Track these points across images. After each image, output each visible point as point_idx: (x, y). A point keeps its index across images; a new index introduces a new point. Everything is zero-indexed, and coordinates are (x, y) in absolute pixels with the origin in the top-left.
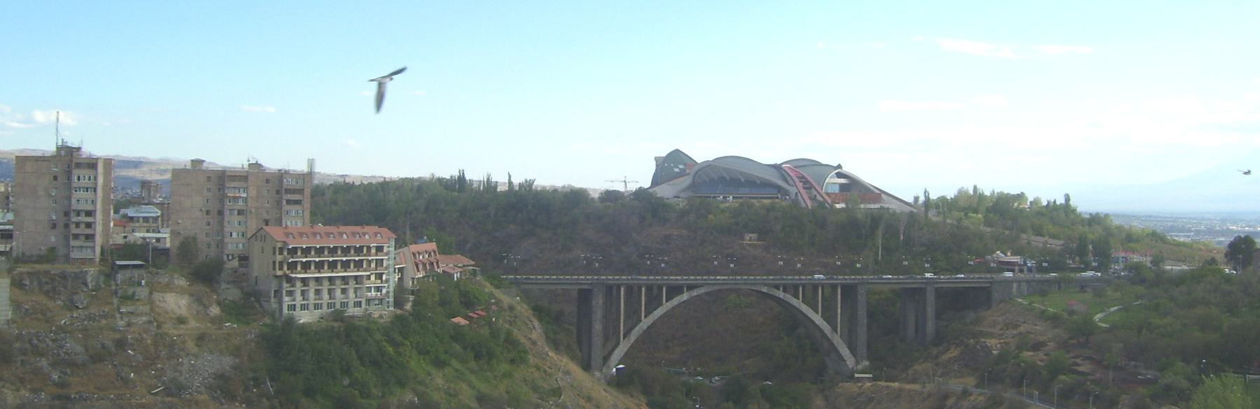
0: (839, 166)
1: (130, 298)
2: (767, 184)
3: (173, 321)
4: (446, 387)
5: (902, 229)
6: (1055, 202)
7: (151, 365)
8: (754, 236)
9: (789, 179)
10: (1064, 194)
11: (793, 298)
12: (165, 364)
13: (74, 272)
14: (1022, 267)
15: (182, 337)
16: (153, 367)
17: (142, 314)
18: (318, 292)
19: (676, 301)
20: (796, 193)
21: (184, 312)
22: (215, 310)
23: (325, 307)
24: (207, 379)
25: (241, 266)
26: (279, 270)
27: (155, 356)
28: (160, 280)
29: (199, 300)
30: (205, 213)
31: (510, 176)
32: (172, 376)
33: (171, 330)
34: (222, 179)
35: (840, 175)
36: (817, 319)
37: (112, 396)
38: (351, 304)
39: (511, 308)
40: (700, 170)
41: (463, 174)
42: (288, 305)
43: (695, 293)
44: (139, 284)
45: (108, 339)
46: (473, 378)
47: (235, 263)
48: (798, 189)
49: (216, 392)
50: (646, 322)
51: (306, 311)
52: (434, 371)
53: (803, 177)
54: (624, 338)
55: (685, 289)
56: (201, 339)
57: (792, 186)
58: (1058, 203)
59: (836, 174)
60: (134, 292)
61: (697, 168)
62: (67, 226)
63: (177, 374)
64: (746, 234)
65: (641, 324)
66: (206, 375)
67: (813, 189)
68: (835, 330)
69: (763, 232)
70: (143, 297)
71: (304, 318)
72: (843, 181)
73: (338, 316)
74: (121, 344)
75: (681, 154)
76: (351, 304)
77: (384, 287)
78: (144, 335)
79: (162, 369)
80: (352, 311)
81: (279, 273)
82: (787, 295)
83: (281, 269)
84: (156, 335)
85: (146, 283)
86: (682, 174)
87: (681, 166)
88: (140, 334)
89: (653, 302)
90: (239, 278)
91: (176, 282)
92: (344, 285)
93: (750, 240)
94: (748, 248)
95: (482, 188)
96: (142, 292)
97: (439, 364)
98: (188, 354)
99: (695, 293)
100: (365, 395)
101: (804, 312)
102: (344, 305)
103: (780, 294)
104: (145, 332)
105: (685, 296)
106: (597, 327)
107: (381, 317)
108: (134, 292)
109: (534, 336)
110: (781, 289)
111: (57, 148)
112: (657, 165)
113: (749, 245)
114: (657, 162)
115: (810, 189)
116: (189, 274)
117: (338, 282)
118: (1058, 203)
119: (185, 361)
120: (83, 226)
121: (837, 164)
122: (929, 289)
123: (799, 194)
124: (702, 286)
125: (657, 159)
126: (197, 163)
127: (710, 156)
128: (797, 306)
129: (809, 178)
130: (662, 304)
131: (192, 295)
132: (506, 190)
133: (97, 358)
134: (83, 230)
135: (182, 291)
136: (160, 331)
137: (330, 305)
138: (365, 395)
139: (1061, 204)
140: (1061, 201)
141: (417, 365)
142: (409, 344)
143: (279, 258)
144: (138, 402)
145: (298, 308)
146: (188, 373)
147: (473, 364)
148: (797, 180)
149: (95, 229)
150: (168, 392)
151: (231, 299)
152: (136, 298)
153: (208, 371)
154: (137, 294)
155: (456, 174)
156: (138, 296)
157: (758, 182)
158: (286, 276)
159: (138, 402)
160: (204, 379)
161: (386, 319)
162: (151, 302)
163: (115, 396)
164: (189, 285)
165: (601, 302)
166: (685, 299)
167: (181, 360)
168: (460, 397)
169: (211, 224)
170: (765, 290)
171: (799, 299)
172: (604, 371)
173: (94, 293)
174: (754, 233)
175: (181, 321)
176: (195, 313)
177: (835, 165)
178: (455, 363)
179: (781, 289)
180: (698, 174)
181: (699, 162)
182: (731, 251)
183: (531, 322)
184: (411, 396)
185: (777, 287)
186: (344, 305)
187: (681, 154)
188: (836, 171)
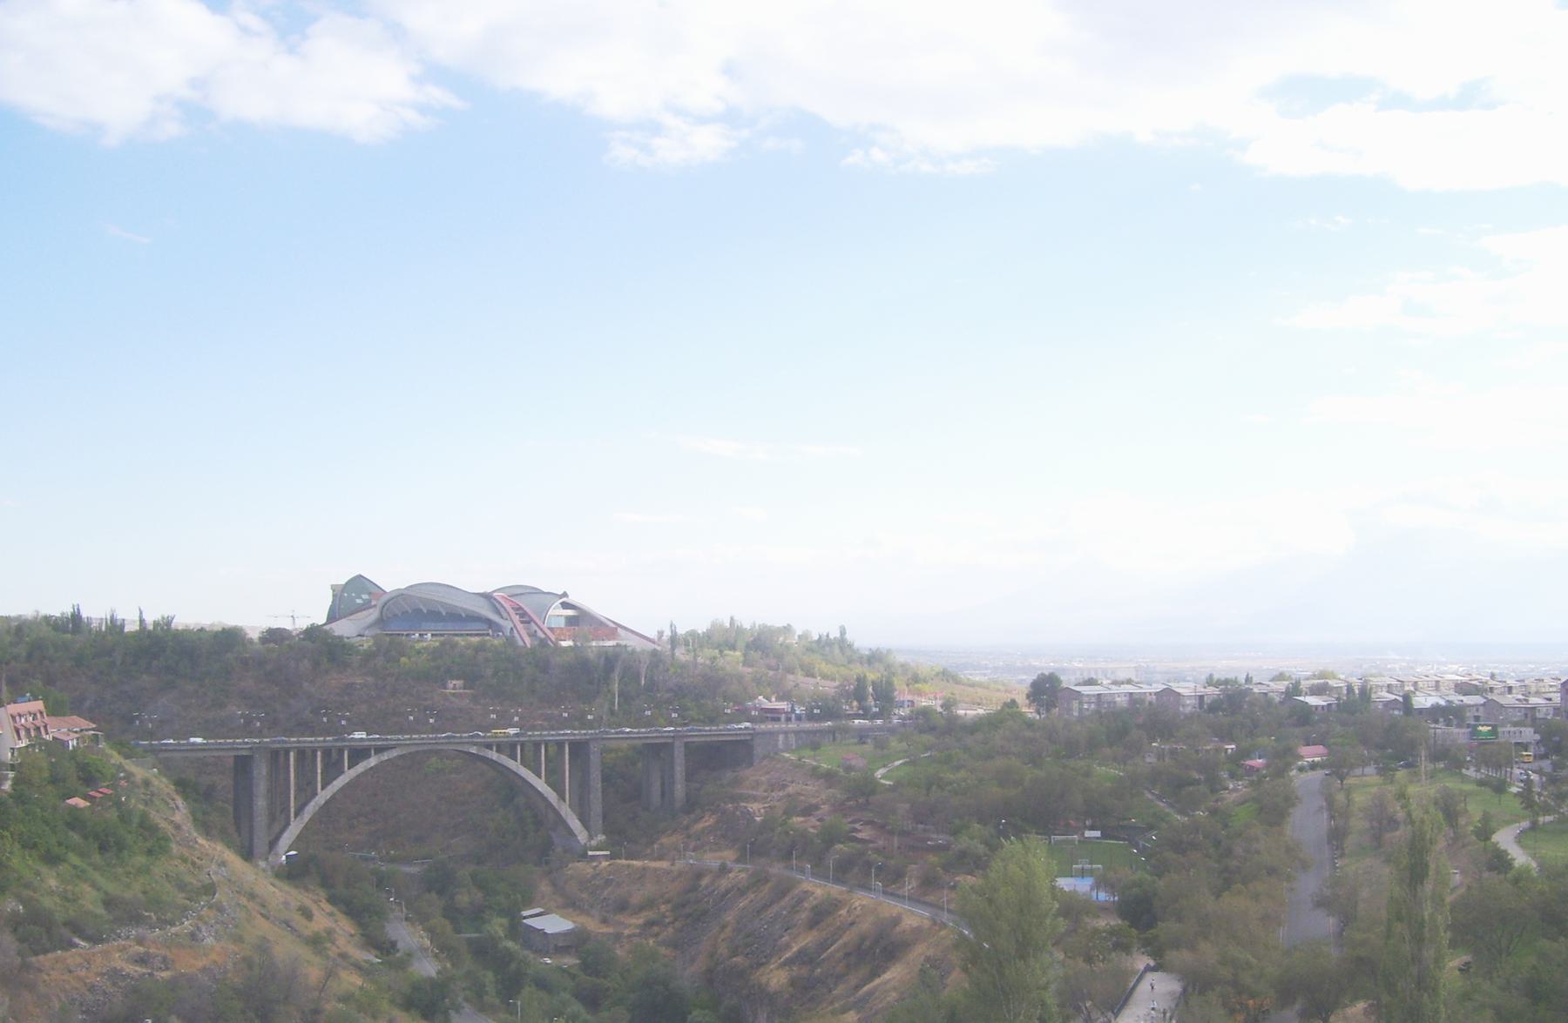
0: (565, 595)
5: (643, 671)
6: (828, 636)
8: (459, 683)
9: (502, 610)
19: (361, 767)
20: (512, 629)
31: (141, 613)
35: (565, 606)
36: (540, 785)
39: (147, 783)
41: (78, 609)
43: (385, 756)
46: (97, 876)
48: (513, 622)
50: (323, 796)
52: (44, 869)
54: (295, 817)
55: (373, 752)
61: (384, 599)
65: (317, 798)
67: (532, 624)
68: (562, 797)
69: (471, 679)
72: (570, 612)
75: (367, 582)
82: (502, 756)
86: (366, 606)
93: (454, 688)
94: (453, 699)
97: (52, 859)
99: (385, 756)
103: (493, 755)
105: (373, 761)
106: (259, 803)
109: (178, 818)
110: (494, 748)
112: (334, 596)
114: (334, 591)
115: (529, 623)
122: (677, 743)
123: (514, 630)
125: (334, 588)
130: (343, 772)
140: (835, 634)
147: (97, 858)
155: (68, 611)
157: (464, 615)
165: (264, 771)
166: (372, 765)
168: (80, 902)
170: (474, 750)
171: (516, 761)
177: (560, 593)
178: (74, 859)
181: (388, 591)
184: (14, 904)
185: (489, 746)
187: (365, 581)
188: (561, 601)
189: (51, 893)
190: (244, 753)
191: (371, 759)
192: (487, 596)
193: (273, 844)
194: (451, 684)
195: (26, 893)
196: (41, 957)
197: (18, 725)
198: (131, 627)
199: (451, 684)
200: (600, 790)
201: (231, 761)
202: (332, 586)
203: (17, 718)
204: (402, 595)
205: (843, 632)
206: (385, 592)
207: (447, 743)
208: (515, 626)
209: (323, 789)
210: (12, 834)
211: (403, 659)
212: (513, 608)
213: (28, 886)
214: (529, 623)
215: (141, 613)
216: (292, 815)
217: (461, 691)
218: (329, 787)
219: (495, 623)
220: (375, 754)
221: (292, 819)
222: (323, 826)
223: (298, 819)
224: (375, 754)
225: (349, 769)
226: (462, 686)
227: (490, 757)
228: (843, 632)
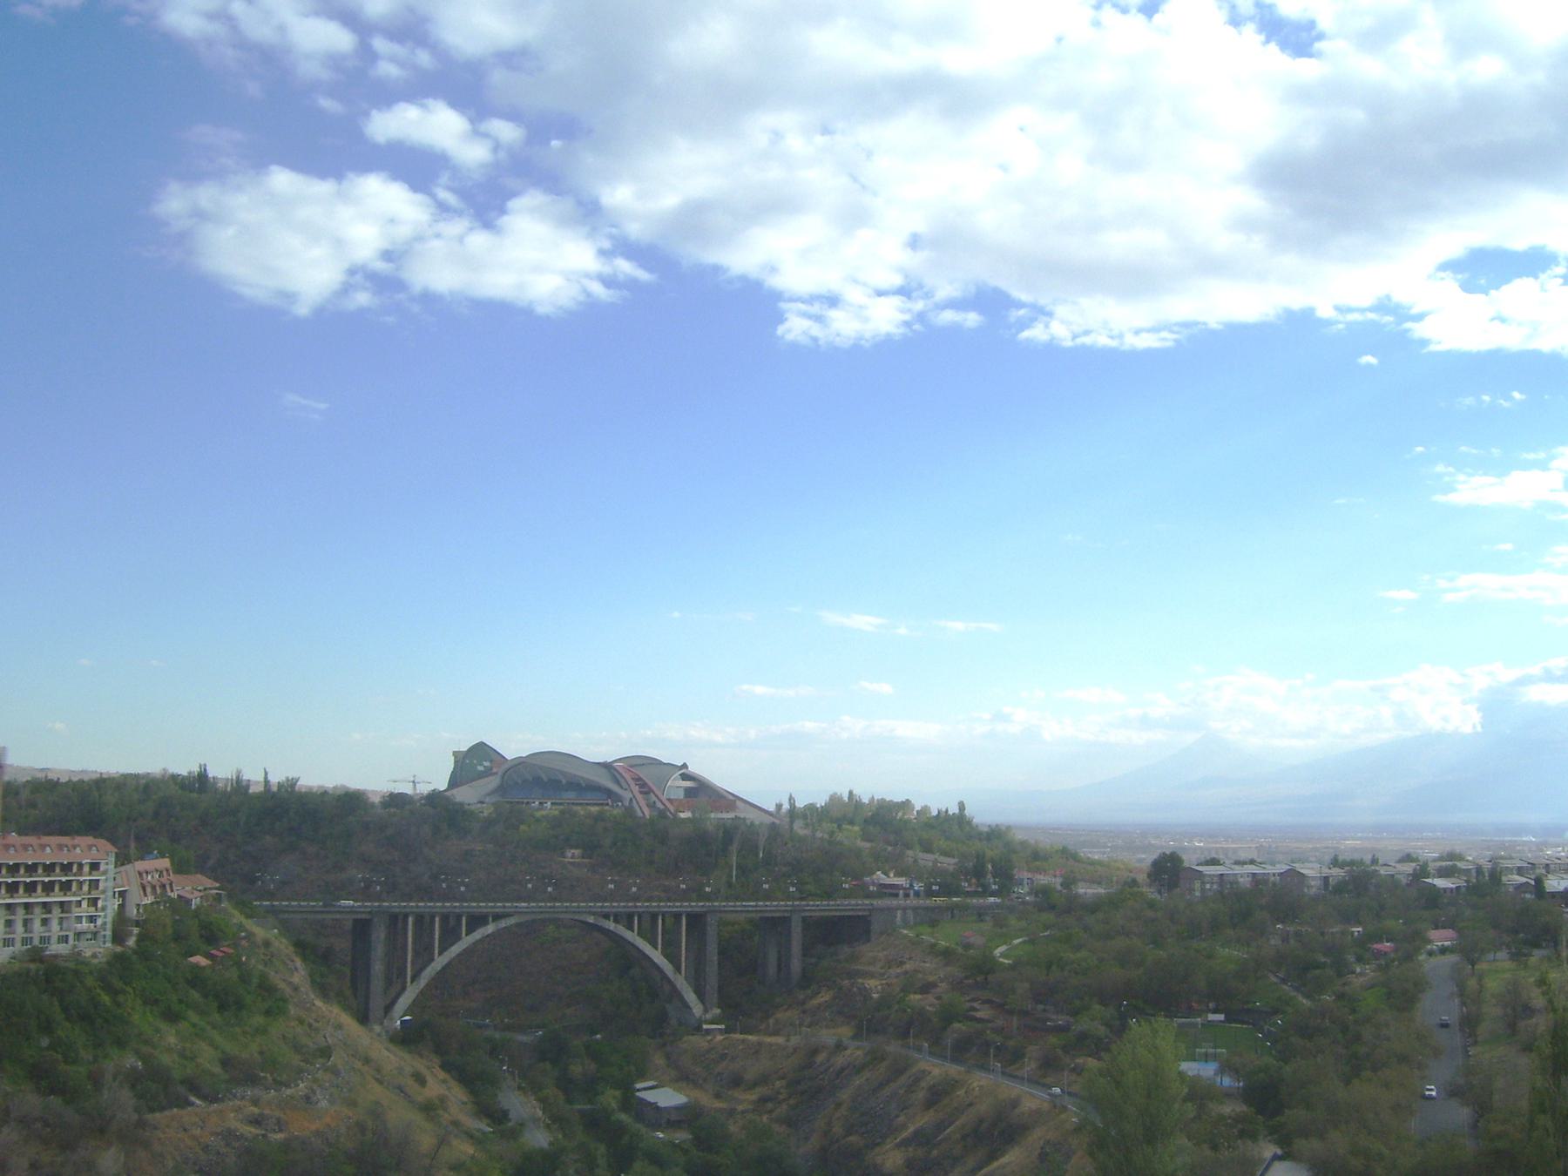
0: (685, 766)
8: (577, 852)
10: (958, 801)
14: (908, 892)
19: (478, 934)
20: (631, 799)
23: (18, 945)
31: (266, 774)
36: (657, 956)
39: (267, 944)
43: (503, 924)
50: (439, 962)
52: (163, 1026)
53: (639, 779)
54: (412, 982)
55: (491, 919)
57: (626, 789)
58: (950, 813)
59: (680, 775)
61: (506, 766)
68: (678, 969)
72: (688, 784)
73: (36, 955)
76: (54, 939)
80: (55, 948)
86: (488, 773)
97: (172, 1017)
99: (503, 924)
103: (611, 925)
105: (490, 928)
107: (94, 956)
110: (612, 918)
112: (455, 762)
114: (455, 757)
117: (37, 910)
118: (950, 813)
123: (634, 800)
125: (455, 754)
130: (459, 938)
137: (25, 941)
139: (954, 814)
147: (216, 1017)
155: (196, 769)
165: (383, 936)
170: (591, 920)
171: (633, 931)
178: (193, 1016)
185: (606, 916)
191: (489, 927)
193: (388, 1008)
194: (569, 853)
196: (157, 1115)
197: (144, 882)
199: (569, 853)
200: (716, 962)
202: (454, 752)
204: (524, 762)
209: (440, 953)
212: (633, 779)
219: (616, 794)
220: (493, 921)
221: (409, 984)
224: (493, 921)
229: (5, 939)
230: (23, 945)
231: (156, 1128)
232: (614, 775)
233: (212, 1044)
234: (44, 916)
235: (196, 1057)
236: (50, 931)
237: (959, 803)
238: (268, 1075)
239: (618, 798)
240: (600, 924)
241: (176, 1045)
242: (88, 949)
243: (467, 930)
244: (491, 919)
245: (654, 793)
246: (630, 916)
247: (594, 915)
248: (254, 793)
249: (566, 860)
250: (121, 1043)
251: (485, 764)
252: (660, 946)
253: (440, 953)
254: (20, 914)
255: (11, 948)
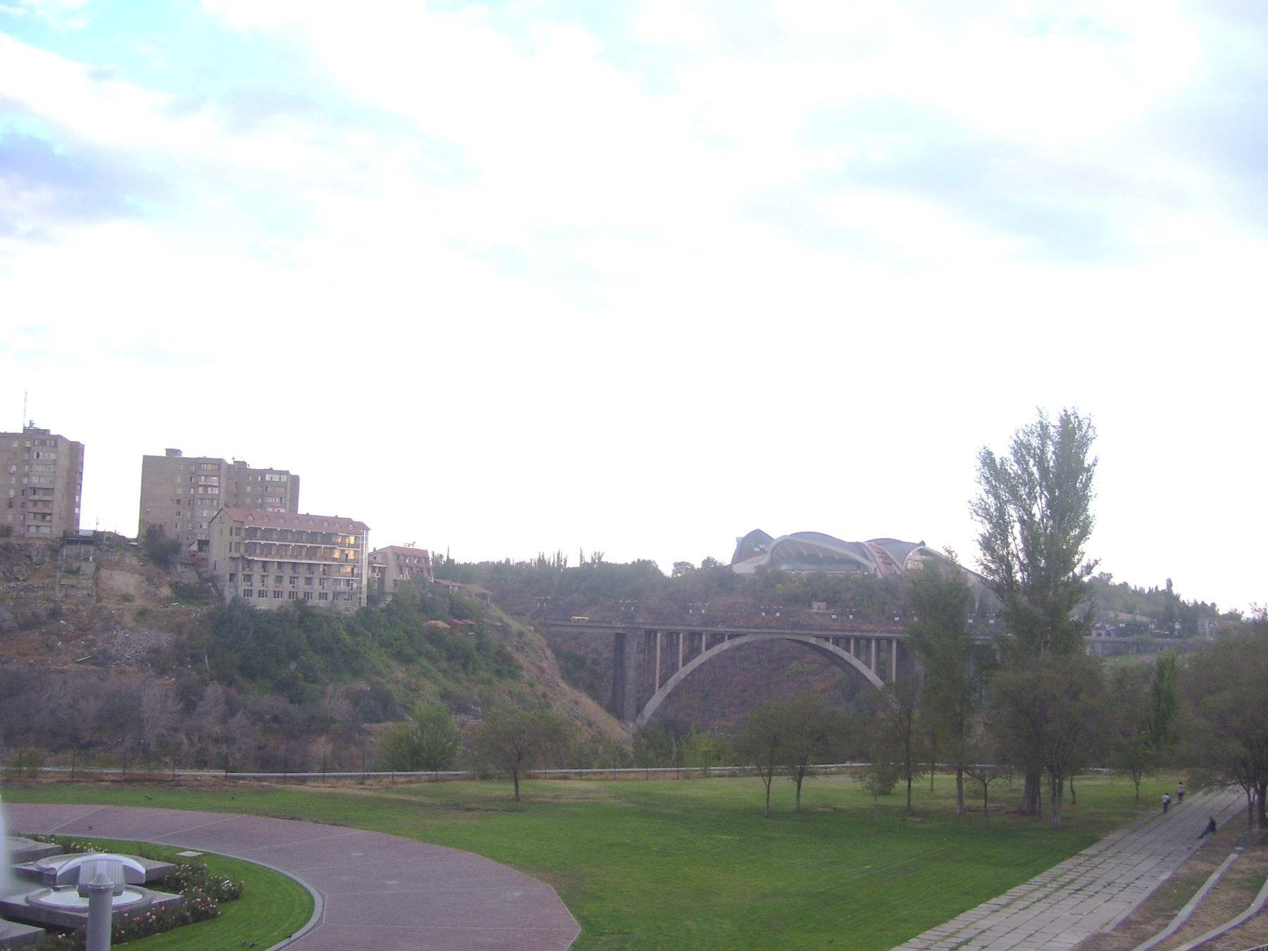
0: (923, 543)
1: (76, 572)
2: (846, 561)
3: (118, 598)
4: (406, 681)
5: (977, 599)
6: (1157, 588)
7: (82, 635)
8: (823, 605)
9: (869, 555)
10: (1166, 578)
11: (844, 651)
12: (97, 636)
13: (18, 544)
14: (1099, 632)
15: (120, 611)
16: (84, 637)
17: (83, 588)
18: (279, 579)
19: (716, 649)
20: (875, 569)
21: (131, 590)
22: (166, 591)
23: (286, 596)
24: (140, 652)
25: (200, 549)
26: (236, 551)
27: (88, 627)
28: (110, 558)
29: (149, 580)
30: (176, 501)
31: (581, 552)
32: (103, 647)
33: (111, 605)
34: (199, 466)
37: (32, 661)
38: (316, 595)
39: (521, 635)
40: (777, 546)
41: (543, 556)
42: (245, 590)
43: (737, 642)
44: (87, 560)
45: (42, 608)
46: (440, 677)
47: (195, 547)
49: (146, 665)
50: (683, 671)
51: (265, 598)
52: (394, 664)
53: (884, 553)
54: (660, 687)
55: (726, 637)
56: (143, 613)
57: (872, 561)
58: (1160, 589)
59: (918, 550)
60: (79, 567)
61: (772, 545)
62: (23, 505)
63: (109, 646)
64: (815, 603)
65: (678, 673)
66: (140, 649)
67: (893, 565)
69: (832, 602)
70: (88, 572)
71: (263, 605)
73: (300, 604)
74: (55, 614)
76: (316, 595)
77: (356, 580)
78: (81, 607)
79: (94, 640)
80: (314, 601)
81: (237, 555)
82: (838, 648)
83: (237, 550)
84: (94, 607)
85: (93, 559)
86: (763, 552)
87: (761, 546)
88: (76, 606)
89: (693, 652)
90: (196, 563)
91: (127, 561)
92: (310, 574)
93: (819, 608)
94: (817, 617)
95: (556, 566)
96: (88, 568)
97: (407, 660)
98: (124, 628)
99: (737, 642)
100: (310, 679)
101: (855, 665)
102: (308, 595)
103: (830, 646)
104: (83, 605)
105: (726, 645)
106: (630, 674)
107: (347, 609)
108: (79, 567)
109: (545, 664)
110: (831, 641)
111: (24, 429)
113: (817, 614)
115: (890, 564)
116: (145, 556)
117: (302, 570)
118: (1160, 589)
119: (121, 634)
120: (40, 505)
121: (920, 541)
123: (878, 570)
124: (743, 635)
126: (172, 453)
127: (788, 531)
128: (848, 660)
129: (890, 555)
130: (701, 653)
131: (142, 575)
132: (577, 568)
133: (30, 624)
134: (41, 508)
135: (133, 570)
136: (98, 604)
137: (291, 594)
138: (310, 679)
139: (1162, 590)
140: (1162, 586)
141: (376, 657)
142: (370, 634)
143: (236, 539)
144: (59, 668)
145: (255, 594)
146: (121, 646)
147: (444, 664)
148: (877, 555)
149: (52, 509)
150: (94, 660)
151: (186, 582)
152: (81, 573)
153: (142, 645)
154: (82, 569)
155: (536, 557)
156: (83, 571)
157: (837, 558)
158: (243, 558)
159: (59, 668)
160: (137, 652)
161: (352, 612)
162: (96, 579)
163: (35, 661)
164: (141, 565)
166: (726, 648)
167: (115, 632)
168: (420, 692)
169: (181, 513)
170: (813, 641)
171: (849, 651)
172: (638, 721)
173: (38, 567)
174: (822, 602)
175: (127, 598)
176: (143, 592)
177: (918, 542)
178: (423, 661)
179: (831, 641)
180: (775, 551)
181: (775, 538)
182: (797, 619)
183: (542, 650)
184: (364, 685)
185: (827, 639)
186: (308, 595)
188: (919, 548)
189: (396, 681)
190: (620, 631)
191: (725, 643)
192: (857, 544)
193: (639, 709)
194: (815, 605)
195: (375, 679)
196: (374, 725)
197: (402, 563)
198: (573, 563)
199: (815, 605)
201: (612, 639)
203: (402, 558)
205: (1169, 584)
206: (773, 539)
207: (790, 634)
208: (877, 565)
209: (684, 665)
210: (373, 635)
211: (779, 586)
213: (380, 674)
214: (890, 564)
215: (581, 552)
216: (657, 685)
217: (825, 611)
218: (689, 664)
219: (863, 565)
220: (729, 639)
221: (657, 689)
222: (701, 713)
223: (661, 689)
224: (729, 639)
225: (706, 650)
226: (825, 607)
227: (827, 648)
228: (1169, 584)
229: (275, 592)
230: (290, 598)
231: (372, 735)
232: (862, 550)
233: (435, 682)
234: (308, 576)
235: (419, 690)
236: (312, 589)
237: (1167, 581)
238: (480, 709)
239: (866, 568)
240: (820, 645)
241: (403, 679)
242: (341, 605)
243: (706, 647)
244: (726, 637)
245: (896, 564)
246: (848, 639)
247: (815, 637)
248: (569, 568)
249: (813, 611)
250: (356, 673)
251: (761, 546)
252: (873, 666)
253: (684, 665)
254: (288, 572)
255: (280, 599)
